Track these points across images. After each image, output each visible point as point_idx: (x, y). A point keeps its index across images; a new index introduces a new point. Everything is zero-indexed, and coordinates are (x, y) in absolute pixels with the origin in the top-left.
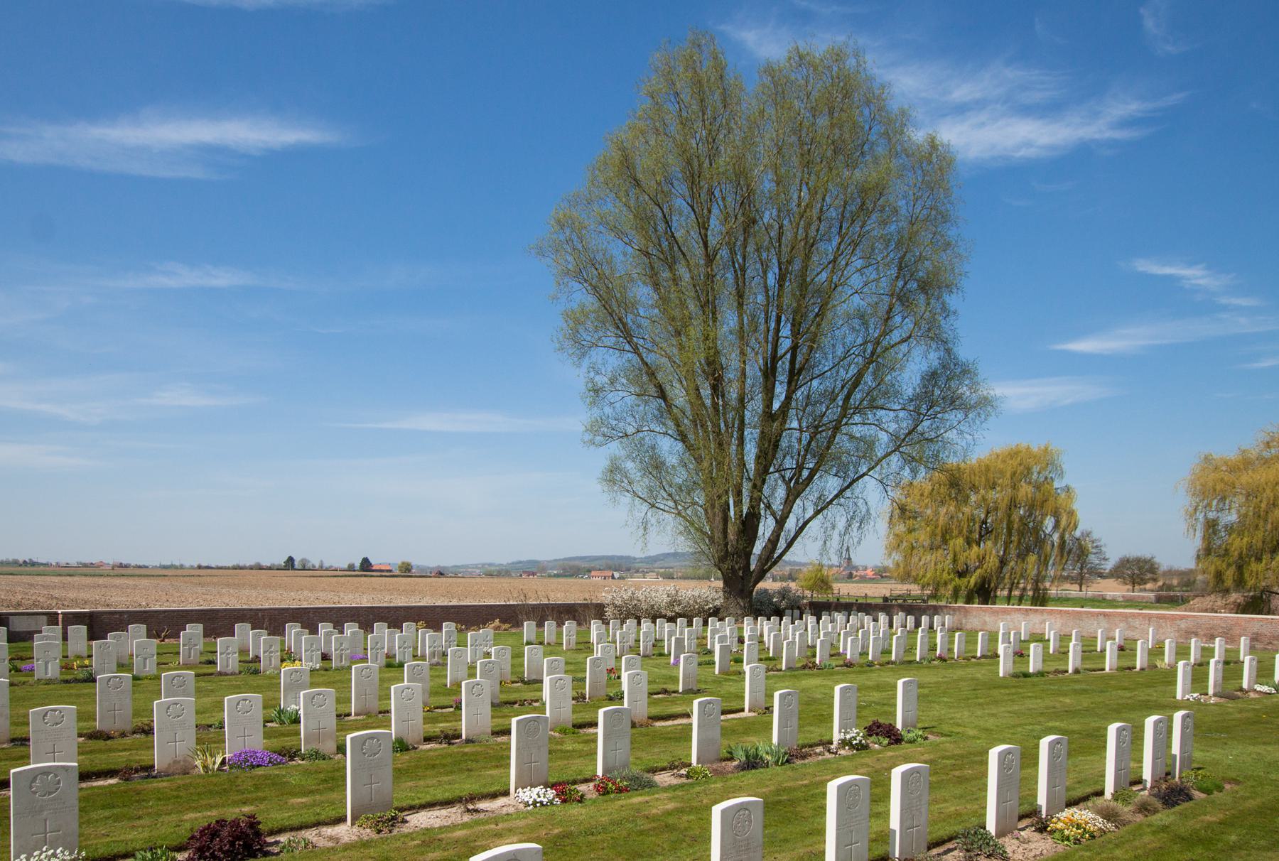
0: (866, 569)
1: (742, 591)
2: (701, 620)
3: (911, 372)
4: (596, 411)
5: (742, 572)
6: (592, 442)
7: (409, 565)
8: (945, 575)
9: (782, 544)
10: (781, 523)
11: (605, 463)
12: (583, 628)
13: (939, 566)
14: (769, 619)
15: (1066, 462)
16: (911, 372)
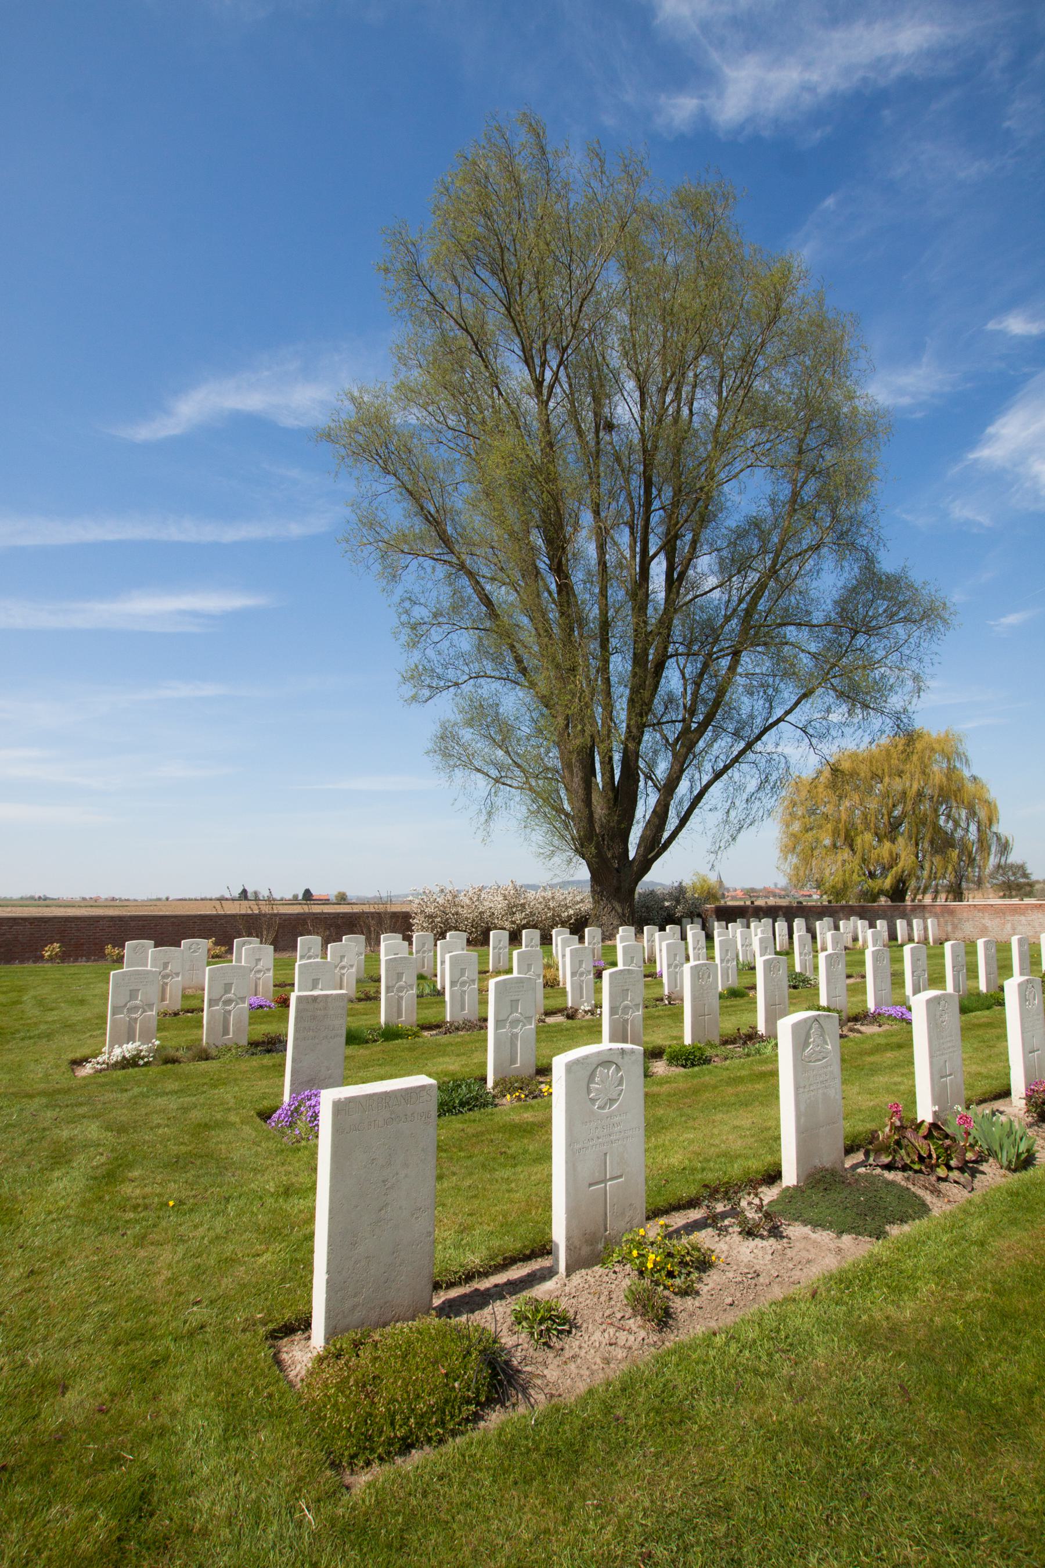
0: (735, 890)
1: (618, 889)
2: (536, 934)
3: (826, 582)
4: (416, 656)
5: (620, 888)
6: (414, 698)
7: (344, 894)
8: (855, 876)
9: (672, 823)
10: (669, 788)
11: (435, 729)
12: (286, 955)
13: (848, 867)
14: (662, 929)
15: (971, 748)
16: (826, 582)
